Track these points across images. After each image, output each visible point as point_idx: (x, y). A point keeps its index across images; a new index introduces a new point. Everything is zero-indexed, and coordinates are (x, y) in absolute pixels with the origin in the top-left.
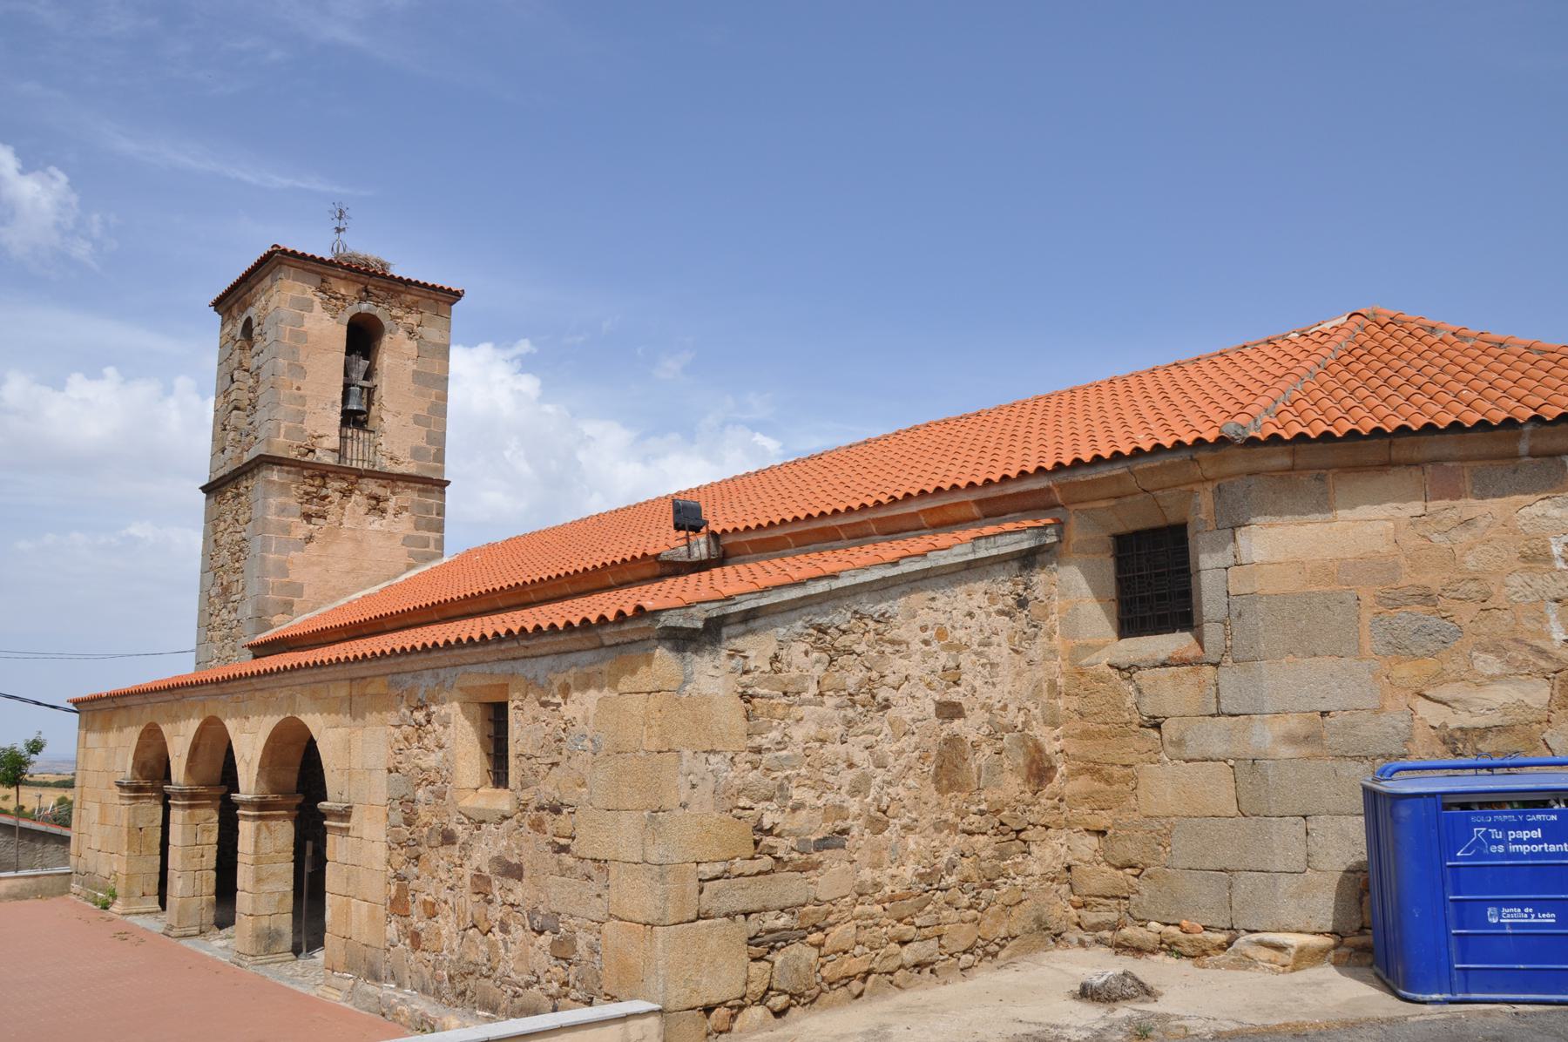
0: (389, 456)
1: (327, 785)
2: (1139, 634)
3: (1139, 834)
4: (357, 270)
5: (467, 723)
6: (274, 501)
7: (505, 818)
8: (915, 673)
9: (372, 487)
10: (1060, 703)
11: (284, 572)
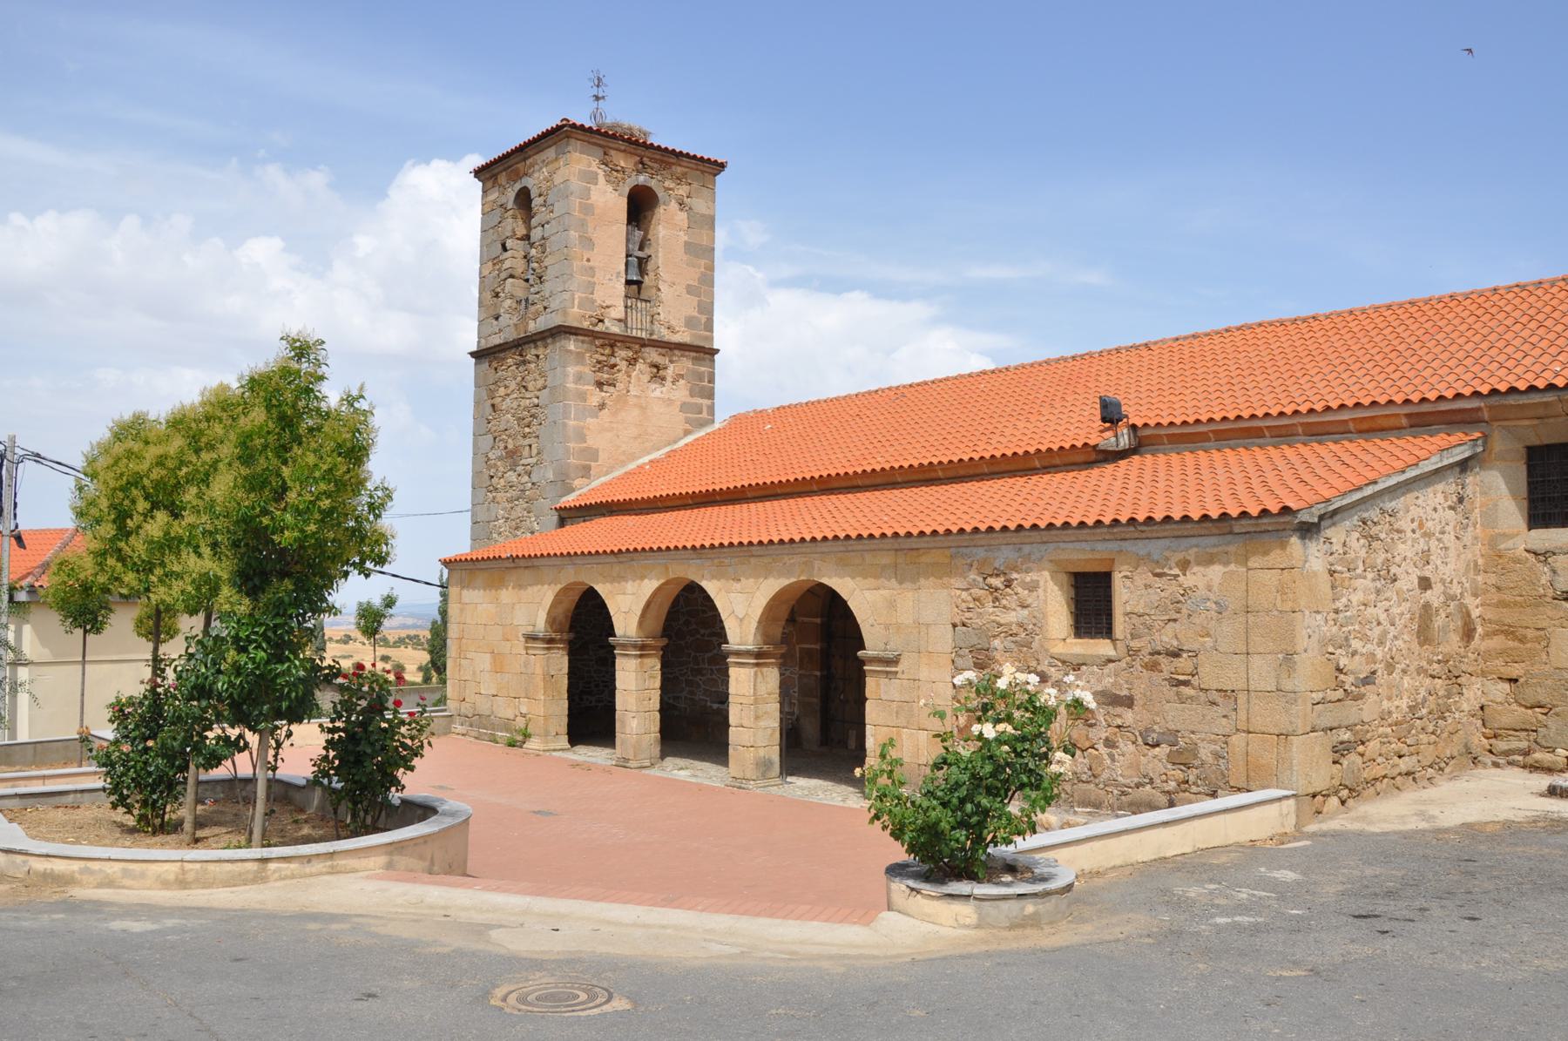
0: (667, 325)
1: (864, 635)
2: (1547, 526)
3: (1549, 682)
4: (636, 143)
5: (1056, 588)
6: (572, 370)
7: (1110, 661)
8: (1409, 555)
9: (653, 355)
10: (1479, 578)
11: (582, 437)
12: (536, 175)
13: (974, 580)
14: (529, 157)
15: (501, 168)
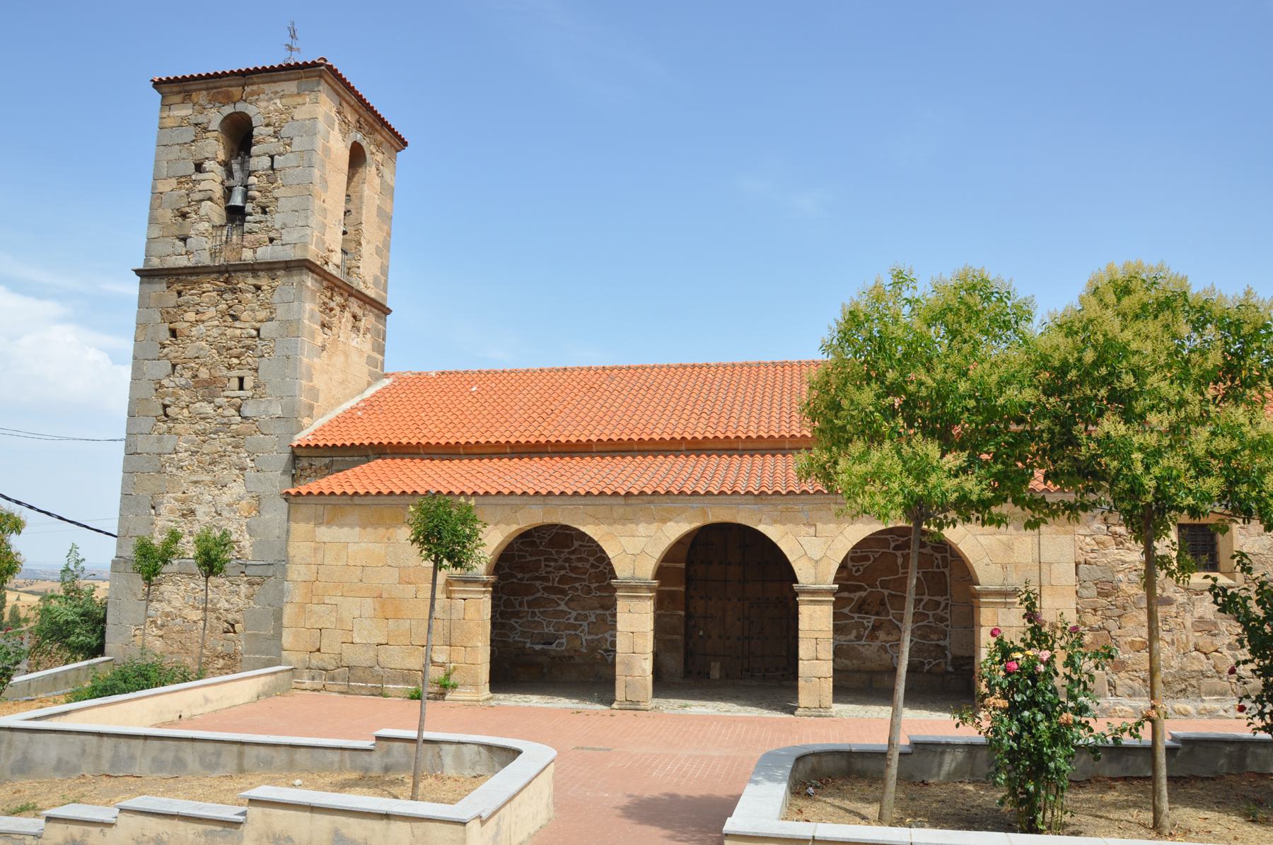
9: (354, 306)
12: (263, 104)
13: (1099, 528)
14: (253, 84)
15: (204, 86)
